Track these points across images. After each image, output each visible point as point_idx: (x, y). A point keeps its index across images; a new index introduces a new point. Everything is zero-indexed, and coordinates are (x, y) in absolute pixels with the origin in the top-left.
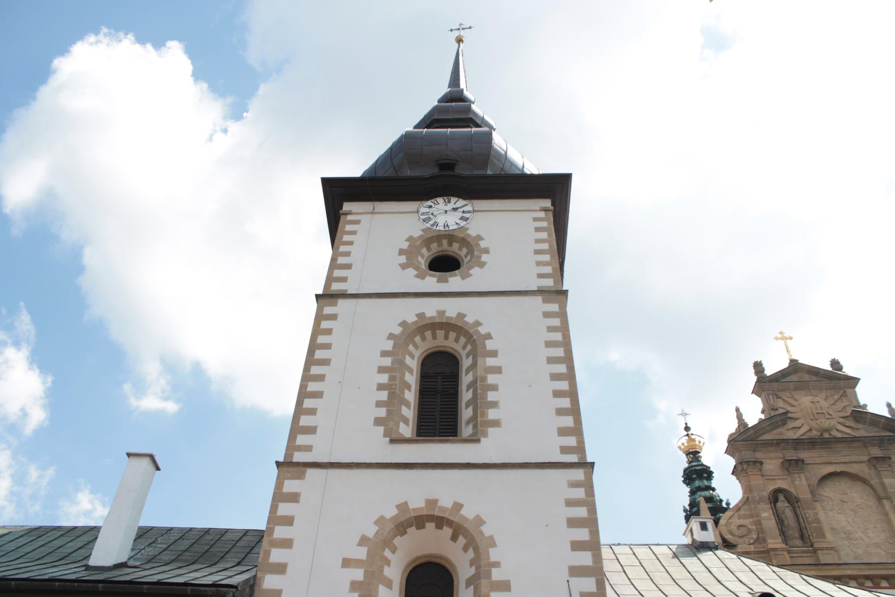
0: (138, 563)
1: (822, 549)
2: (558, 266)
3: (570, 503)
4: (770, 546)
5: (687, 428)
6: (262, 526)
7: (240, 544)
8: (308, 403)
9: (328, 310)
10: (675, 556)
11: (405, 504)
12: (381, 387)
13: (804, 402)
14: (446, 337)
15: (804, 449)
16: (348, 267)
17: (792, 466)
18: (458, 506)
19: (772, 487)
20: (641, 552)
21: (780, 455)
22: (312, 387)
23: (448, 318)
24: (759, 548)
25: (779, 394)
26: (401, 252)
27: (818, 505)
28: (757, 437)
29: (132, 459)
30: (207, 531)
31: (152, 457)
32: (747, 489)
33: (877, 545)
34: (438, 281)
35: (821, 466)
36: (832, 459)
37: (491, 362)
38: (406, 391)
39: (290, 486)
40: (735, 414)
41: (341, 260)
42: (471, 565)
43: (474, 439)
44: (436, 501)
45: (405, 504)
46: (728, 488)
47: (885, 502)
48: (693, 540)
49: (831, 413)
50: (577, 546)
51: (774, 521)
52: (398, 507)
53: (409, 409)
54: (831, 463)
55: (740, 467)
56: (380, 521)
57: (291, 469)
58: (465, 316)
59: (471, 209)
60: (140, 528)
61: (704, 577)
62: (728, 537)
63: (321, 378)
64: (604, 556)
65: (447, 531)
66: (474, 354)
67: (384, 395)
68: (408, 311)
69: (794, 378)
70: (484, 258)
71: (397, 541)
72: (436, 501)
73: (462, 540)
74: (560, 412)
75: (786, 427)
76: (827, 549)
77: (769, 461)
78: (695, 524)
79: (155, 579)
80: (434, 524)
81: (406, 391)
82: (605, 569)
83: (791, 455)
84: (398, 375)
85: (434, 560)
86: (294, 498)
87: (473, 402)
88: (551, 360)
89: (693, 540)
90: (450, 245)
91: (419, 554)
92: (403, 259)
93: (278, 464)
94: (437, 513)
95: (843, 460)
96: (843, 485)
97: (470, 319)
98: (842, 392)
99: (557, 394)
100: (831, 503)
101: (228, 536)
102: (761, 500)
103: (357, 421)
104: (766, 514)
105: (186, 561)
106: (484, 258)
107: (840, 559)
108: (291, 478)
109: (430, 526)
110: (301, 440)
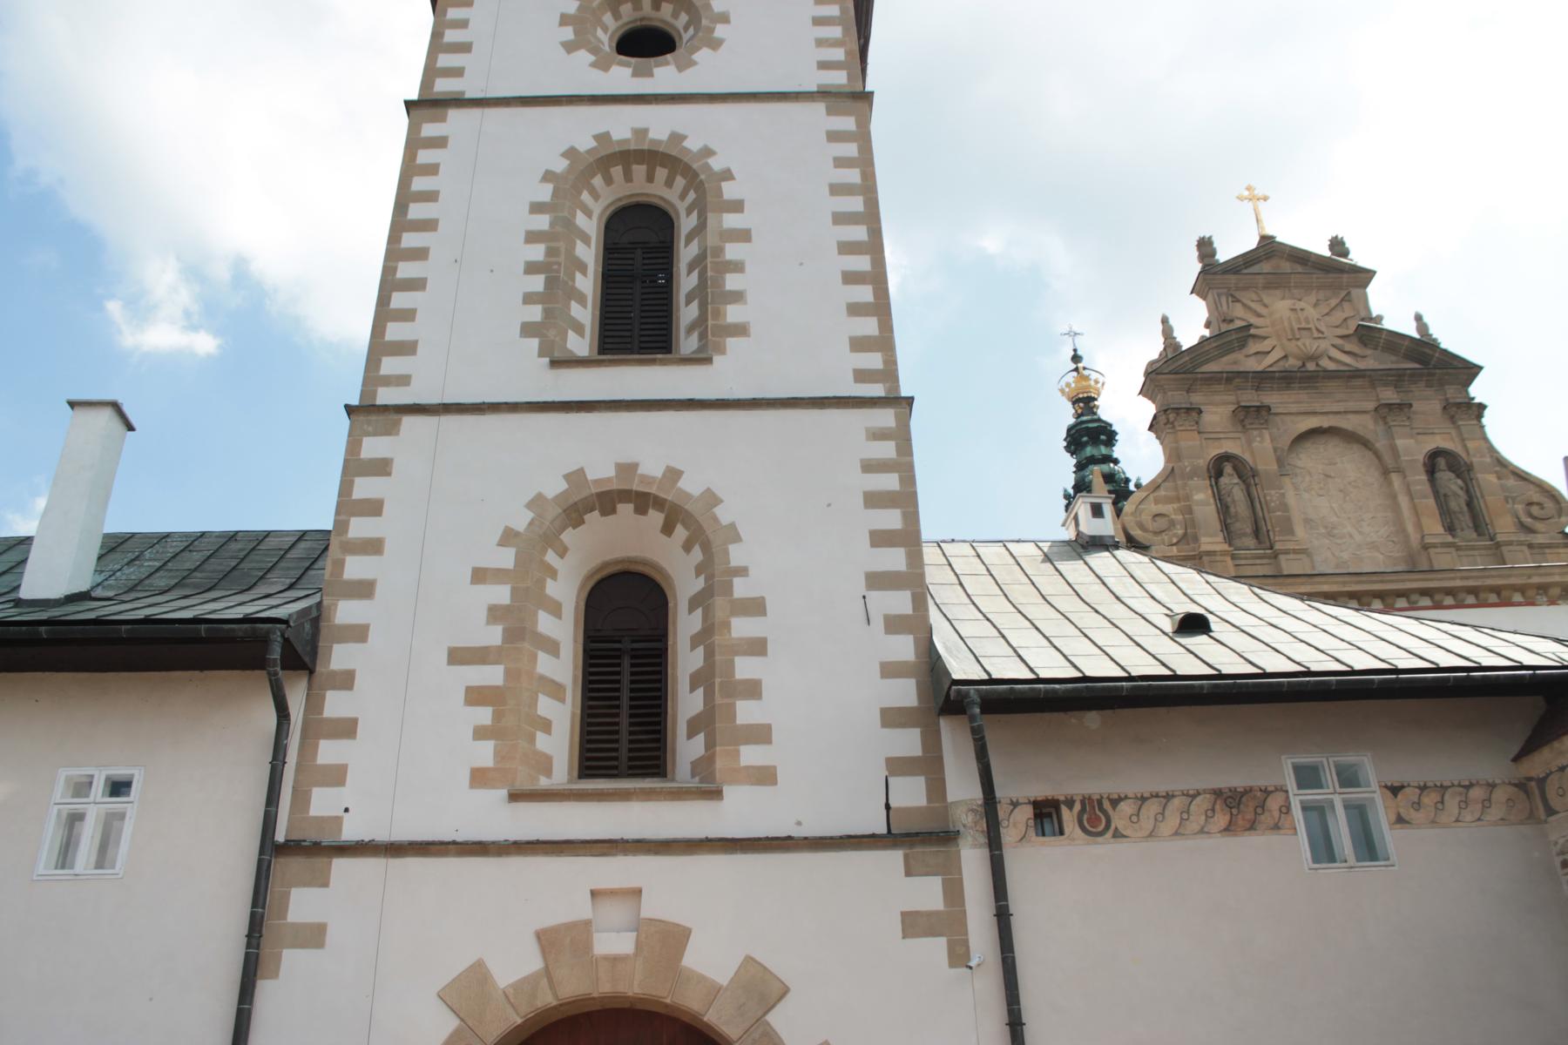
0: (110, 594)
1: (1287, 552)
2: (856, 47)
3: (869, 467)
4: (1204, 548)
5: (1076, 358)
6: (330, 527)
7: (292, 554)
8: (399, 300)
9: (429, 130)
10: (1047, 558)
11: (581, 472)
12: (531, 268)
13: (1281, 314)
14: (650, 178)
15: (1272, 389)
16: (465, 48)
17: (1251, 416)
18: (673, 474)
19: (1215, 451)
20: (991, 553)
21: (1232, 398)
22: (405, 270)
23: (653, 141)
24: (1187, 550)
25: (1237, 294)
26: (565, 20)
27: (1286, 480)
28: (1195, 367)
29: (79, 412)
30: (233, 536)
31: (116, 406)
32: (1173, 455)
33: (1373, 546)
34: (635, 74)
35: (1300, 418)
36: (1318, 407)
37: (731, 221)
38: (578, 276)
39: (373, 447)
40: (1160, 327)
41: (451, 36)
42: (698, 575)
43: (701, 358)
44: (635, 466)
45: (581, 472)
46: (1140, 456)
47: (1394, 477)
48: (1079, 534)
49: (1323, 329)
50: (880, 539)
51: (1213, 507)
52: (567, 477)
53: (585, 307)
54: (1315, 413)
55: (1162, 419)
56: (537, 502)
57: (374, 418)
58: (684, 137)
60: (107, 536)
61: (1094, 592)
62: (1136, 533)
63: (420, 254)
64: (927, 559)
65: (656, 518)
66: (700, 206)
67: (537, 283)
68: (581, 129)
69: (1265, 267)
70: (720, 31)
71: (568, 536)
72: (635, 466)
73: (680, 532)
74: (855, 310)
75: (1245, 351)
76: (1295, 551)
77: (1214, 409)
78: (1082, 508)
79: (140, 614)
80: (631, 506)
81: (578, 276)
82: (928, 580)
83: (1250, 398)
84: (562, 245)
85: (633, 568)
86: (382, 467)
87: (700, 293)
88: (840, 219)
89: (1079, 534)
91: (608, 557)
92: (568, 33)
93: (350, 409)
94: (636, 486)
95: (1335, 409)
97: (693, 144)
98: (1343, 293)
99: (850, 278)
100: (1308, 479)
101: (271, 543)
102: (1194, 473)
103: (488, 329)
104: (1202, 496)
105: (195, 586)
106: (720, 31)
107: (1313, 567)
108: (375, 434)
109: (625, 509)
110: (390, 365)
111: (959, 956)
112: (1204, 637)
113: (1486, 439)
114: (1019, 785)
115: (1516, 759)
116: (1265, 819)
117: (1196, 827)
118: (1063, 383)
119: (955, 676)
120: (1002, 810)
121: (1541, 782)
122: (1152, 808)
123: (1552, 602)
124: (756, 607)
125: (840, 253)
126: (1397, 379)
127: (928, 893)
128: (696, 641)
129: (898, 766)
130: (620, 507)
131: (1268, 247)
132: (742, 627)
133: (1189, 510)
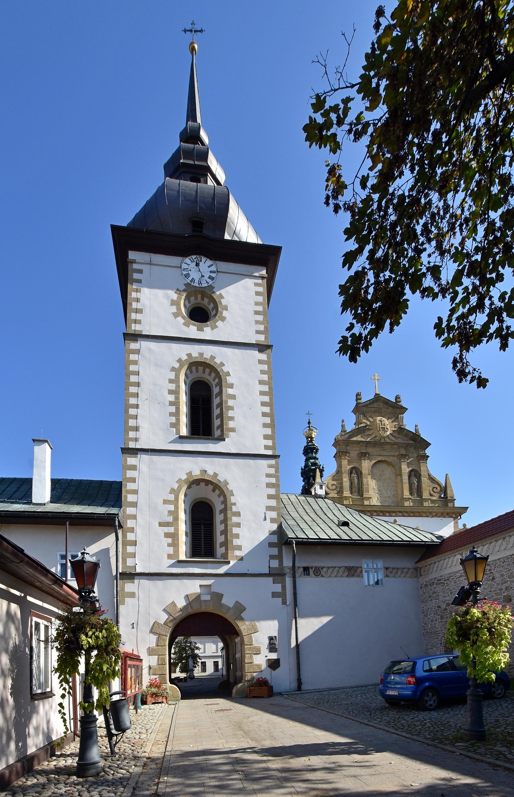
17: (363, 455)
54: (381, 455)
59: (215, 269)
65: (211, 487)
69: (375, 405)
90: (202, 299)
91: (197, 497)
96: (383, 466)
97: (218, 361)
109: (203, 484)
111: (284, 602)
112: (346, 527)
113: (427, 467)
114: (301, 563)
115: (416, 563)
116: (356, 574)
117: (340, 575)
118: (304, 431)
119: (289, 536)
120: (296, 569)
121: (421, 568)
122: (331, 570)
123: (433, 517)
124: (238, 514)
125: (142, 270)
126: (406, 446)
127: (278, 588)
128: (222, 522)
129: (272, 557)
130: (201, 483)
131: (378, 398)
132: (235, 519)
133: (342, 483)
